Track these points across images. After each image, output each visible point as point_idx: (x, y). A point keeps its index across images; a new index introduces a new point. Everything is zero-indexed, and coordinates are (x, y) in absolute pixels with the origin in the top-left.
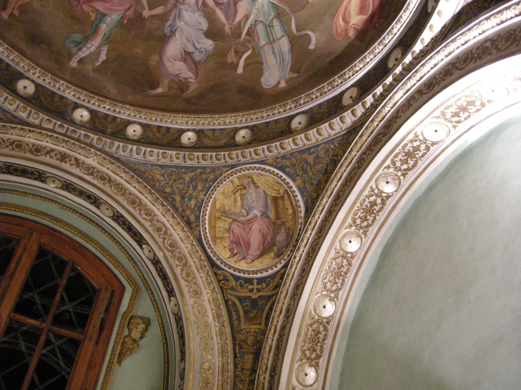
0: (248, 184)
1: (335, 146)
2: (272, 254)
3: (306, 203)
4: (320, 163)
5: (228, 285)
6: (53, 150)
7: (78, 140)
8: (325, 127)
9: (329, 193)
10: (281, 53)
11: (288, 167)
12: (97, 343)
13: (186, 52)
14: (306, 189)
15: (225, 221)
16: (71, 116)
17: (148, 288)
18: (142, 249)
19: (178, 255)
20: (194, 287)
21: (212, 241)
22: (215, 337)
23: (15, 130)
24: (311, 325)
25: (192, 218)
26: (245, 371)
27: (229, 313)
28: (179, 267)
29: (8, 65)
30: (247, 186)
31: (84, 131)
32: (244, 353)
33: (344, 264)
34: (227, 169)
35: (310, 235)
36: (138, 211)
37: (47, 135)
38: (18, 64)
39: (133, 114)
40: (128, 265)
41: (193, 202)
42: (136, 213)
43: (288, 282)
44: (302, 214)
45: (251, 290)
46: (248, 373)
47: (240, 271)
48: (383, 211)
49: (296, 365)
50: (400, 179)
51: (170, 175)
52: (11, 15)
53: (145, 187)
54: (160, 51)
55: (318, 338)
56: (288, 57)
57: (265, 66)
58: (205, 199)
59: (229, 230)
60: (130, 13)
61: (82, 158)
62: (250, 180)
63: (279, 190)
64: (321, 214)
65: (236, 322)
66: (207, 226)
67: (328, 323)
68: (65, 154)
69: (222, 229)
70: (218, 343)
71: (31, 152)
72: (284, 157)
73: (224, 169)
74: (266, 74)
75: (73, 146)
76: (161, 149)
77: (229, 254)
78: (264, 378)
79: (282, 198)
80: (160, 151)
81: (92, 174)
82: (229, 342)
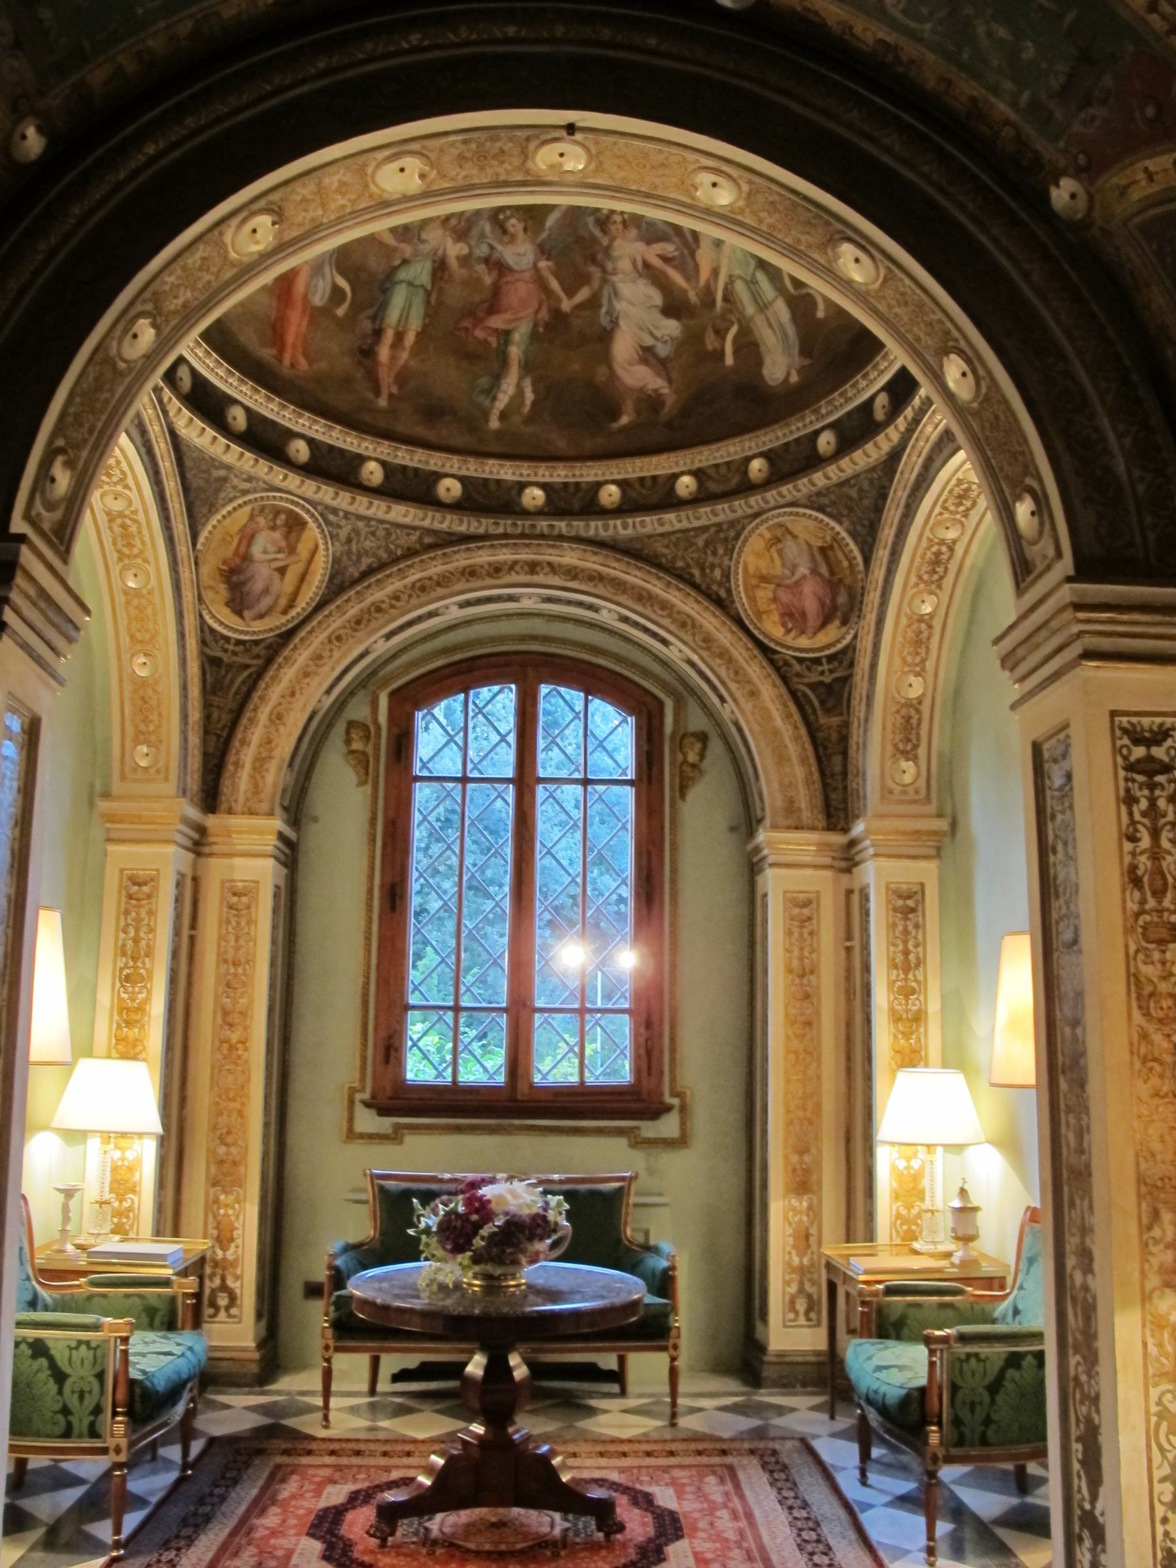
2: (837, 622)
3: (862, 551)
6: (516, 562)
7: (542, 536)
8: (858, 455)
10: (781, 325)
13: (642, 347)
16: (519, 504)
20: (748, 687)
24: (898, 712)
25: (723, 594)
29: (416, 470)
38: (427, 463)
41: (717, 573)
44: (861, 567)
45: (822, 673)
49: (889, 764)
51: (676, 545)
52: (391, 396)
54: (606, 357)
56: (791, 331)
57: (762, 348)
59: (775, 600)
60: (544, 315)
65: (812, 718)
67: (920, 703)
71: (490, 575)
74: (768, 361)
77: (782, 631)
81: (575, 578)
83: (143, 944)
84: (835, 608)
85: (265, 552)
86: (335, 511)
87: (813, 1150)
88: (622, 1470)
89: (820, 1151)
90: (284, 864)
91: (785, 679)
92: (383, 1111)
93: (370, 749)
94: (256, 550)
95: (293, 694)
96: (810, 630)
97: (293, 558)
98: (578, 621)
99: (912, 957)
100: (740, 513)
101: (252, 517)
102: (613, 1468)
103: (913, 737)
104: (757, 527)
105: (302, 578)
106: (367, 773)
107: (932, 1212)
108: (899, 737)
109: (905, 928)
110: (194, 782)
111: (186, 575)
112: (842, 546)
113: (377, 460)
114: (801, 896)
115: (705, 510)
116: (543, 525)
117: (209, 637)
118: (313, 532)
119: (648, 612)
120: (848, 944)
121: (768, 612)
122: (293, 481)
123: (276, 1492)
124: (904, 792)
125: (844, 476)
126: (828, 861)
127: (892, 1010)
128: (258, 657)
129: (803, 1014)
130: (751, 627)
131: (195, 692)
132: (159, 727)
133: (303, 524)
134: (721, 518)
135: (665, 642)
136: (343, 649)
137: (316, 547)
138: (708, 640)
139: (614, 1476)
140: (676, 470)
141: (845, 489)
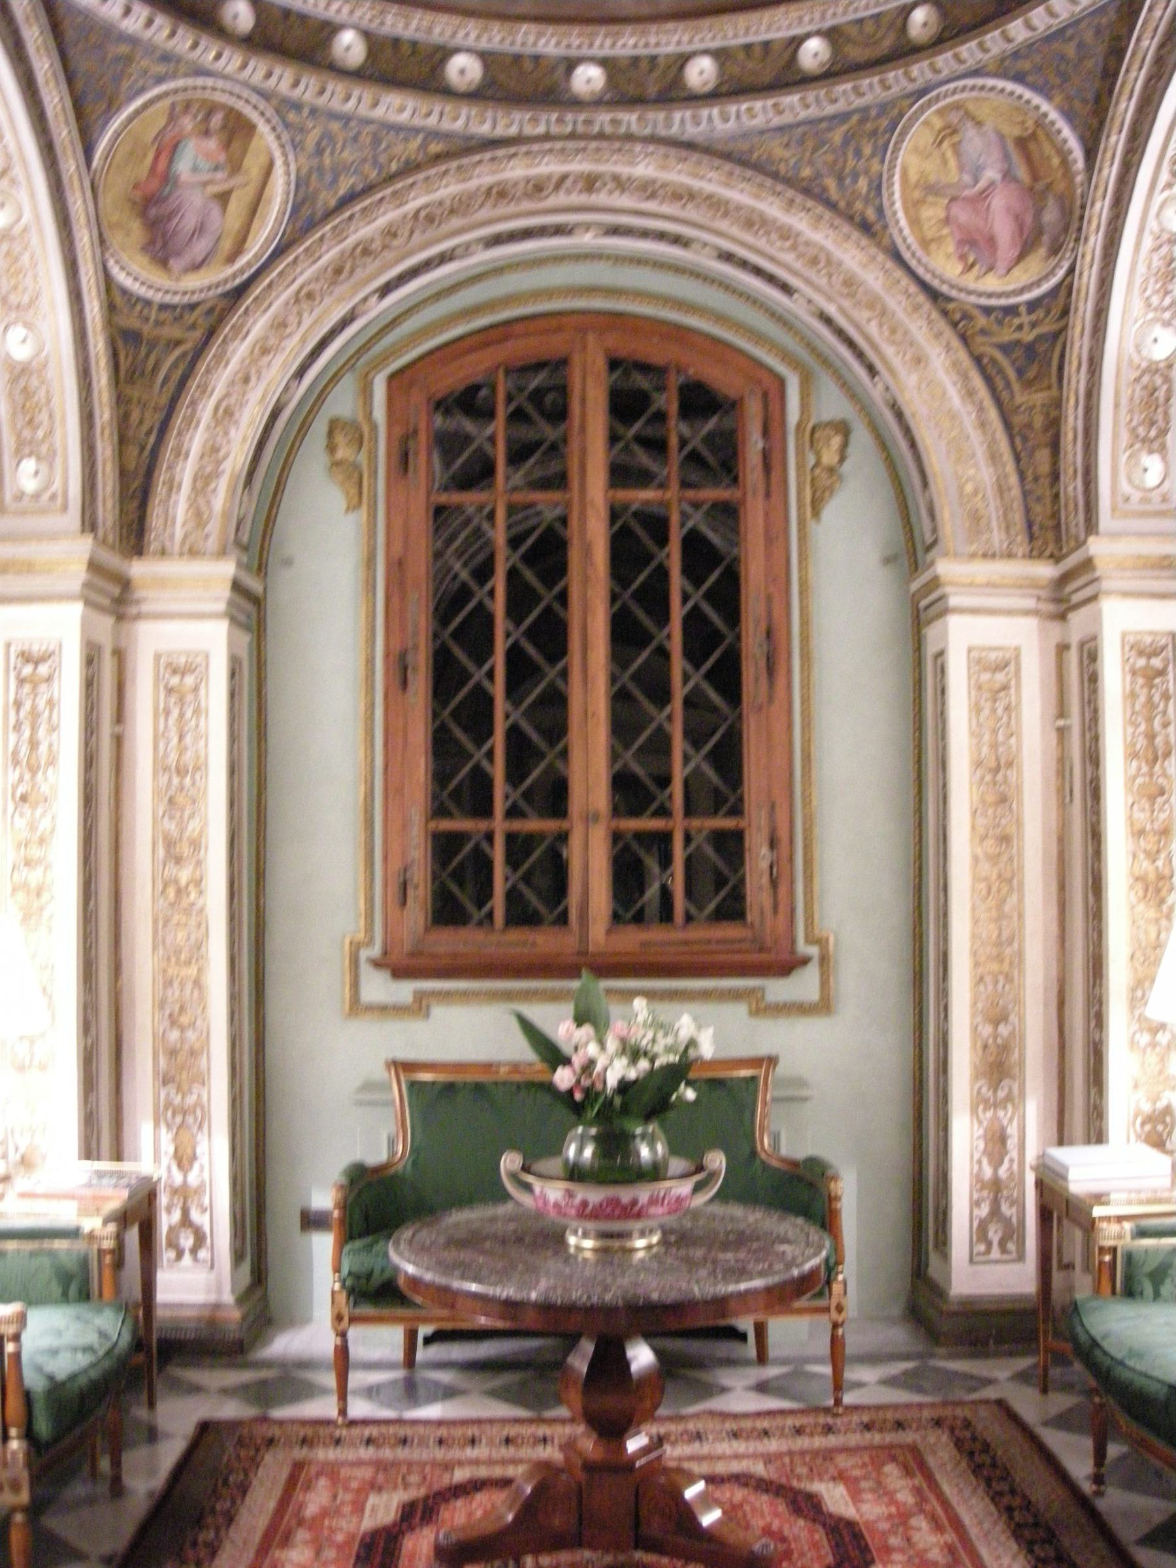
2: (1042, 251)
3: (1082, 139)
6: (564, 177)
7: (601, 136)
12: (768, 495)
24: (1137, 380)
25: (871, 214)
26: (1042, 480)
29: (414, 44)
32: (1034, 449)
34: (911, 100)
35: (1101, 209)
39: (686, 38)
41: (863, 184)
42: (762, 243)
44: (1080, 164)
45: (1020, 327)
47: (990, 295)
51: (801, 142)
55: (1157, 399)
59: (947, 221)
61: (624, 170)
63: (1023, 122)
65: (1005, 395)
71: (527, 195)
72: (1016, 55)
73: (907, 102)
78: (1075, 488)
81: (652, 196)
83: (43, 749)
84: (1039, 231)
85: (195, 169)
86: (297, 106)
87: (1013, 1018)
88: (768, 1459)
89: (1021, 1019)
90: (247, 628)
91: (964, 339)
92: (400, 972)
93: (363, 458)
94: (183, 166)
95: (246, 380)
96: (1001, 266)
97: (238, 180)
98: (659, 265)
99: (1159, 740)
100: (895, 90)
101: (172, 117)
102: (754, 1456)
103: (1159, 417)
104: (922, 109)
105: (254, 209)
106: (360, 493)
109: (1150, 698)
110: (107, 510)
111: (78, 205)
112: (1052, 135)
113: (356, 27)
114: (993, 656)
115: (844, 87)
116: (603, 119)
117: (119, 300)
118: (266, 137)
119: (762, 243)
120: (1061, 723)
121: (939, 240)
122: (232, 60)
123: (301, 1506)
124: (1145, 500)
125: (1056, 23)
126: (1030, 603)
128: (193, 327)
130: (913, 263)
131: (102, 379)
132: (50, 433)
133: (251, 128)
134: (868, 99)
135: (786, 288)
136: (317, 312)
137: (271, 165)
138: (850, 283)
139: (759, 1469)
140: (798, 31)
141: (1056, 45)
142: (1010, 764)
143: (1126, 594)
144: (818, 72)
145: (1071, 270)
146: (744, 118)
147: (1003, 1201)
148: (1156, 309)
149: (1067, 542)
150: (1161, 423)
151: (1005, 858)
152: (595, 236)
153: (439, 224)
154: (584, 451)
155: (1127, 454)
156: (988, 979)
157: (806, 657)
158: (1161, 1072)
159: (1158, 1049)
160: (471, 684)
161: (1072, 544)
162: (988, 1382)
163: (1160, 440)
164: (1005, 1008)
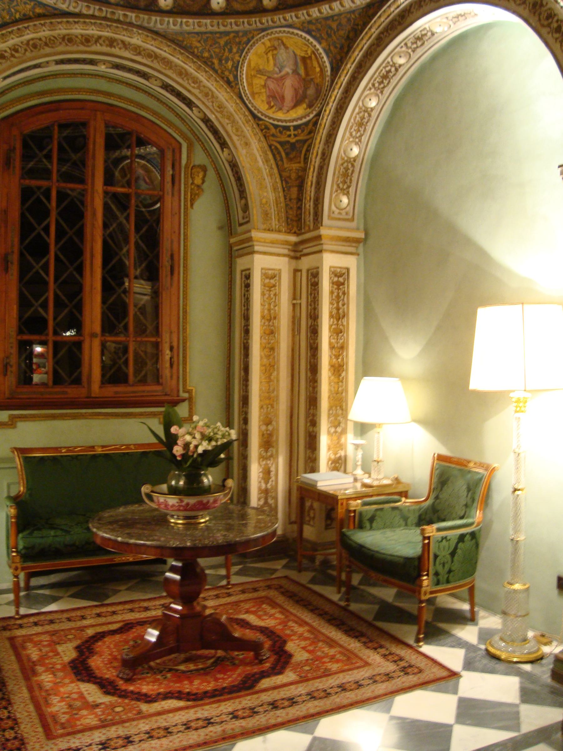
0: (278, 45)
1: (356, 17)
2: (305, 106)
3: (331, 63)
4: (342, 30)
5: (269, 133)
6: (100, 37)
9: (352, 60)
11: (313, 31)
14: (331, 51)
15: (260, 78)
17: (199, 139)
18: (192, 110)
19: (226, 114)
21: (251, 95)
22: (266, 177)
23: (63, 24)
24: (342, 164)
25: (231, 78)
26: (292, 201)
27: (274, 156)
28: (229, 125)
30: (277, 47)
31: (122, 10)
32: (290, 187)
33: (365, 116)
34: (258, 32)
35: (337, 93)
36: (187, 82)
37: (91, 23)
40: (177, 122)
41: (230, 64)
42: (185, 83)
43: (321, 131)
45: (290, 136)
46: (295, 201)
47: (278, 120)
48: (396, 76)
49: (334, 195)
50: (410, 55)
51: (206, 41)
53: (188, 57)
58: (241, 60)
59: (265, 86)
61: (127, 39)
62: (280, 41)
63: (306, 51)
64: (346, 76)
65: (280, 163)
66: (245, 84)
67: (355, 161)
68: (111, 38)
69: (258, 86)
70: (270, 183)
71: (82, 43)
72: (310, 22)
73: (255, 33)
75: (116, 30)
76: (196, 19)
77: (267, 106)
78: (310, 206)
79: (310, 58)
80: (195, 21)
81: (139, 54)
82: (278, 180)
87: (274, 423)
89: (277, 423)
99: (341, 311)
103: (348, 181)
107: (378, 462)
108: (341, 180)
109: (338, 293)
114: (270, 272)
121: (259, 93)
124: (340, 213)
126: (286, 252)
127: (330, 343)
129: (269, 343)
134: (241, 28)
141: (329, 22)
142: (275, 318)
143: (333, 252)
144: (220, 11)
145: (318, 115)
146: (184, 26)
147: (269, 498)
148: (353, 137)
149: (304, 228)
150: (348, 183)
151: (272, 357)
152: (107, 68)
153: (39, 50)
154: (94, 166)
155: (336, 194)
156: (265, 406)
157: (185, 266)
158: (338, 443)
159: (337, 434)
160: (34, 270)
161: (307, 228)
162: (275, 570)
163: (347, 190)
164: (271, 418)
